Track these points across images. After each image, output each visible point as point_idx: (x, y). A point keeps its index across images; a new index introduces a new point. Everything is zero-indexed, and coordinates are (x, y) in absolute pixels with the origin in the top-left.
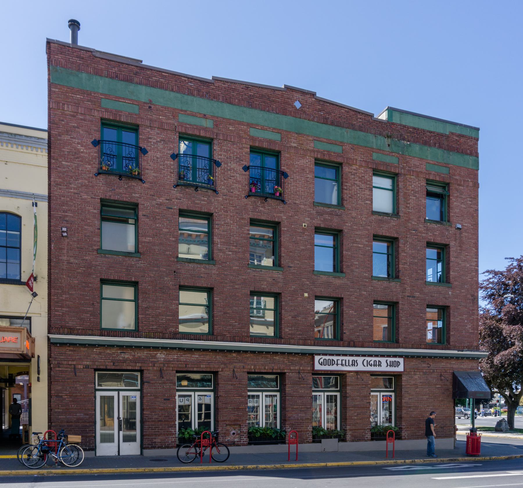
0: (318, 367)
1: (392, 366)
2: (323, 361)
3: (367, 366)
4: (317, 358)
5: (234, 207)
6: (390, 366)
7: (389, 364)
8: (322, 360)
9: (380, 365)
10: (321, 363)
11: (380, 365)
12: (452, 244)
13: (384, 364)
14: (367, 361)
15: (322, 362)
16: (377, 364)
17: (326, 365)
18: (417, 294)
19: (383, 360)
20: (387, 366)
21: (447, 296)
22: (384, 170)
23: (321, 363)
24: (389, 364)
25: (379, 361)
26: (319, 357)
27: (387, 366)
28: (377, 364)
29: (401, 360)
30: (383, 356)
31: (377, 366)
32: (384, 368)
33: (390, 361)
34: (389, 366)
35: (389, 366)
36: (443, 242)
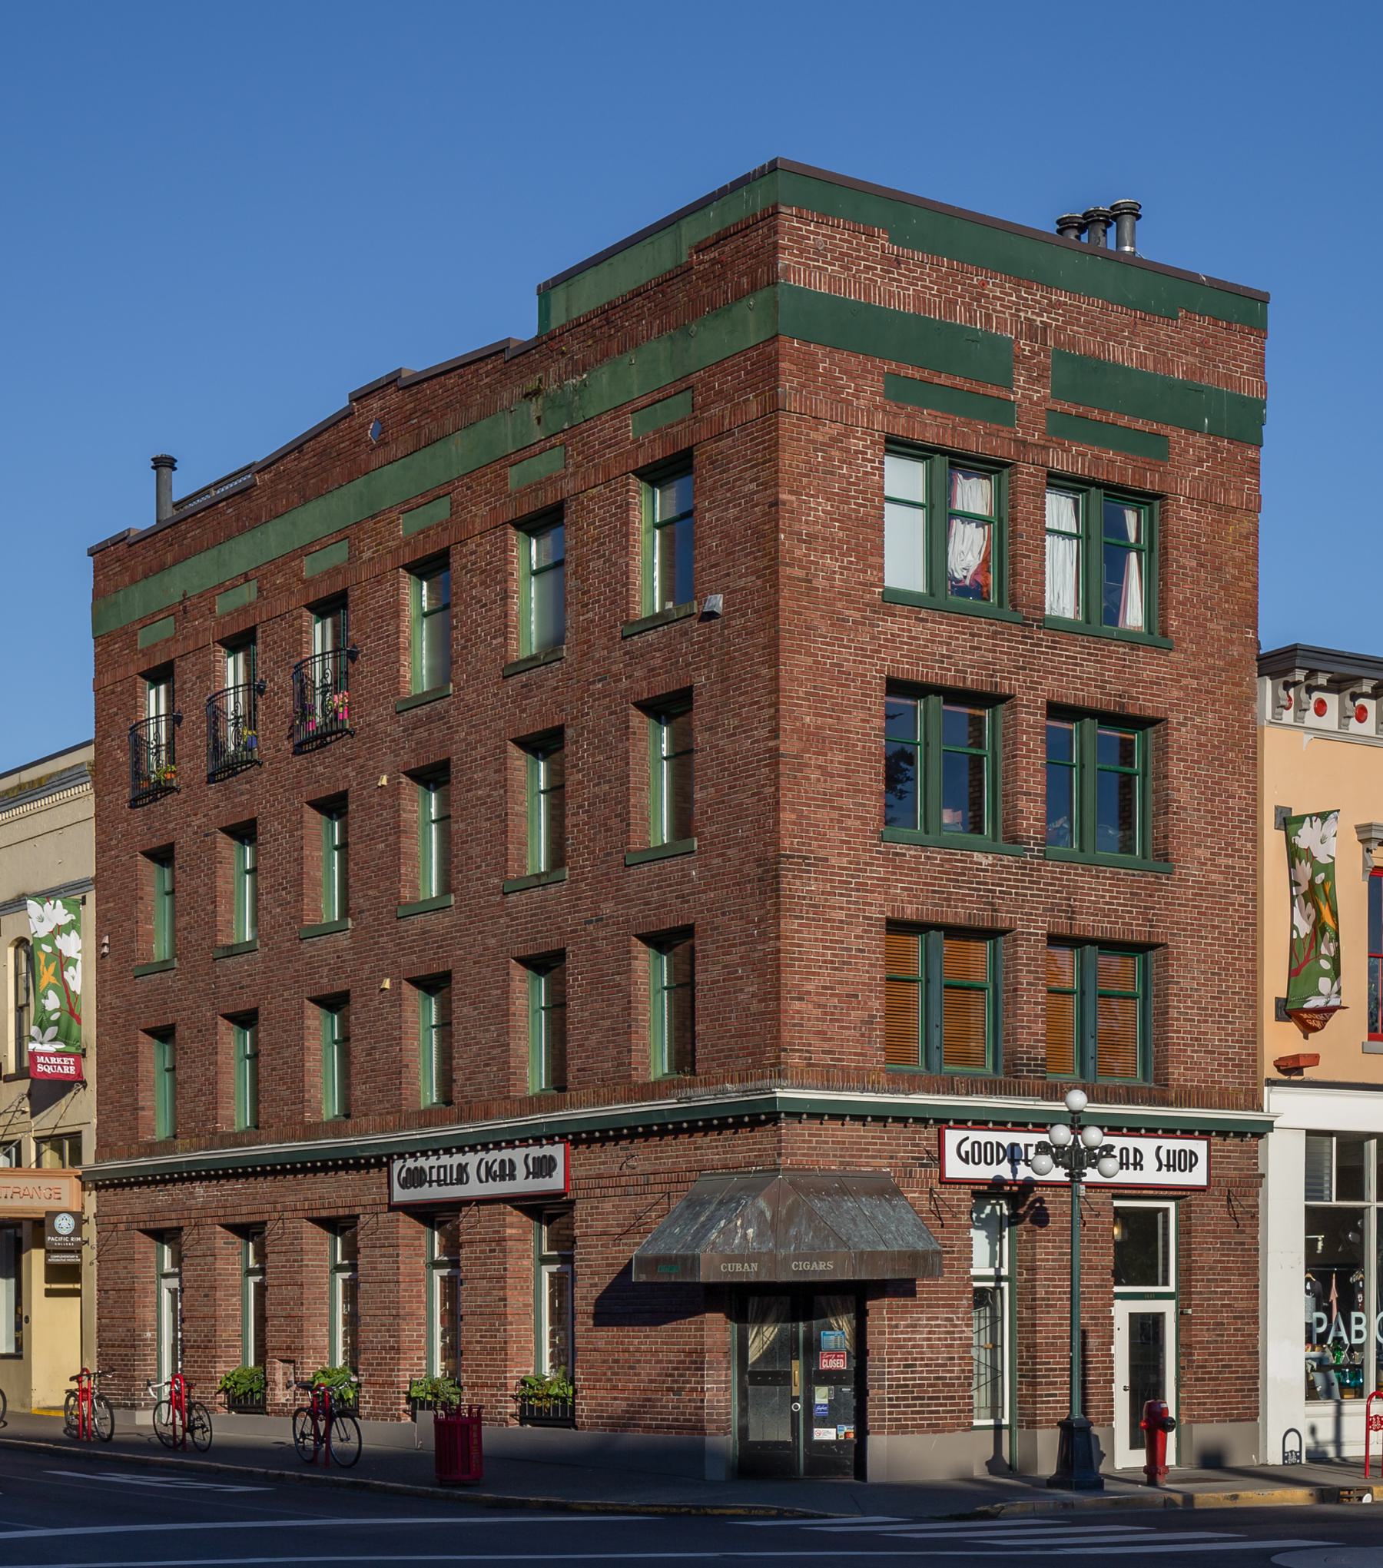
0: (955, 1168)
1: (1174, 1166)
2: (969, 1149)
3: (487, 1181)
4: (952, 1137)
5: (753, 795)
6: (1168, 1166)
7: (1165, 1162)
8: (966, 1147)
9: (1138, 1165)
10: (964, 1155)
11: (1138, 1165)
12: (700, 680)
13: (1149, 1161)
14: (487, 1163)
15: (967, 1153)
16: (1131, 1160)
17: (980, 1162)
18: (607, 908)
19: (1147, 1145)
20: (1159, 1169)
21: (687, 889)
22: (1014, 535)
23: (964, 1155)
24: (1165, 1162)
25: (1136, 1150)
26: (961, 1134)
27: (1159, 1169)
28: (1131, 1160)
29: (1200, 1147)
30: (1151, 1132)
31: (1131, 1167)
32: (522, 1184)
33: (1168, 1151)
34: (1164, 1169)
35: (1164, 1169)
36: (675, 687)
